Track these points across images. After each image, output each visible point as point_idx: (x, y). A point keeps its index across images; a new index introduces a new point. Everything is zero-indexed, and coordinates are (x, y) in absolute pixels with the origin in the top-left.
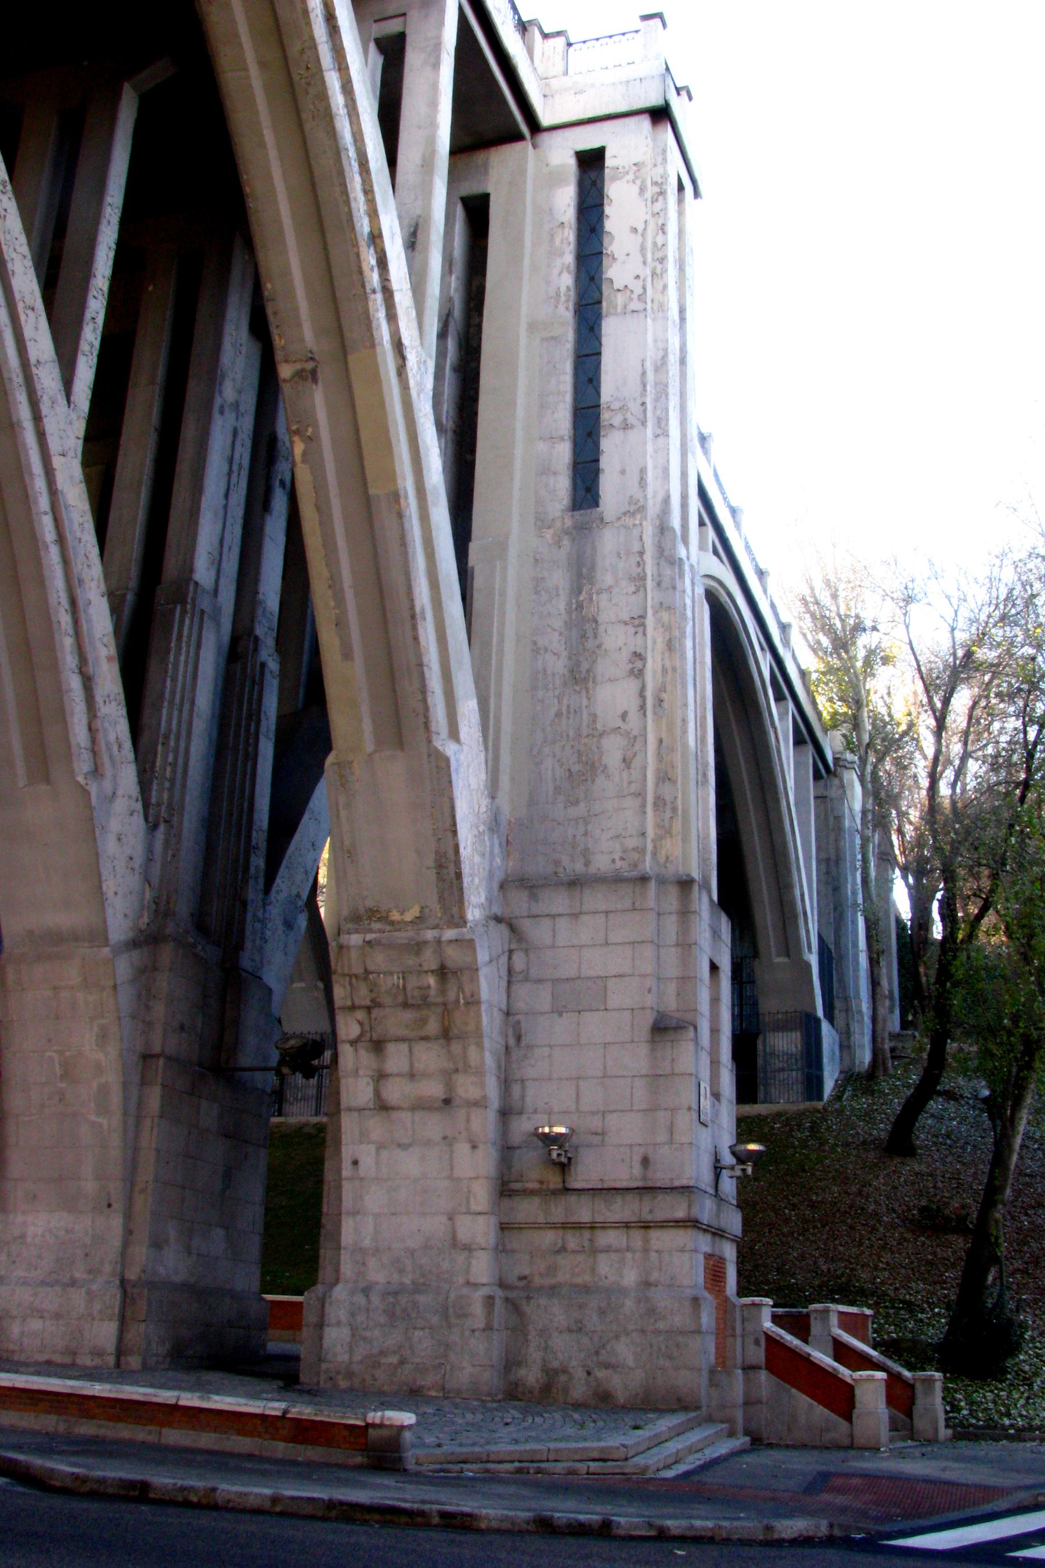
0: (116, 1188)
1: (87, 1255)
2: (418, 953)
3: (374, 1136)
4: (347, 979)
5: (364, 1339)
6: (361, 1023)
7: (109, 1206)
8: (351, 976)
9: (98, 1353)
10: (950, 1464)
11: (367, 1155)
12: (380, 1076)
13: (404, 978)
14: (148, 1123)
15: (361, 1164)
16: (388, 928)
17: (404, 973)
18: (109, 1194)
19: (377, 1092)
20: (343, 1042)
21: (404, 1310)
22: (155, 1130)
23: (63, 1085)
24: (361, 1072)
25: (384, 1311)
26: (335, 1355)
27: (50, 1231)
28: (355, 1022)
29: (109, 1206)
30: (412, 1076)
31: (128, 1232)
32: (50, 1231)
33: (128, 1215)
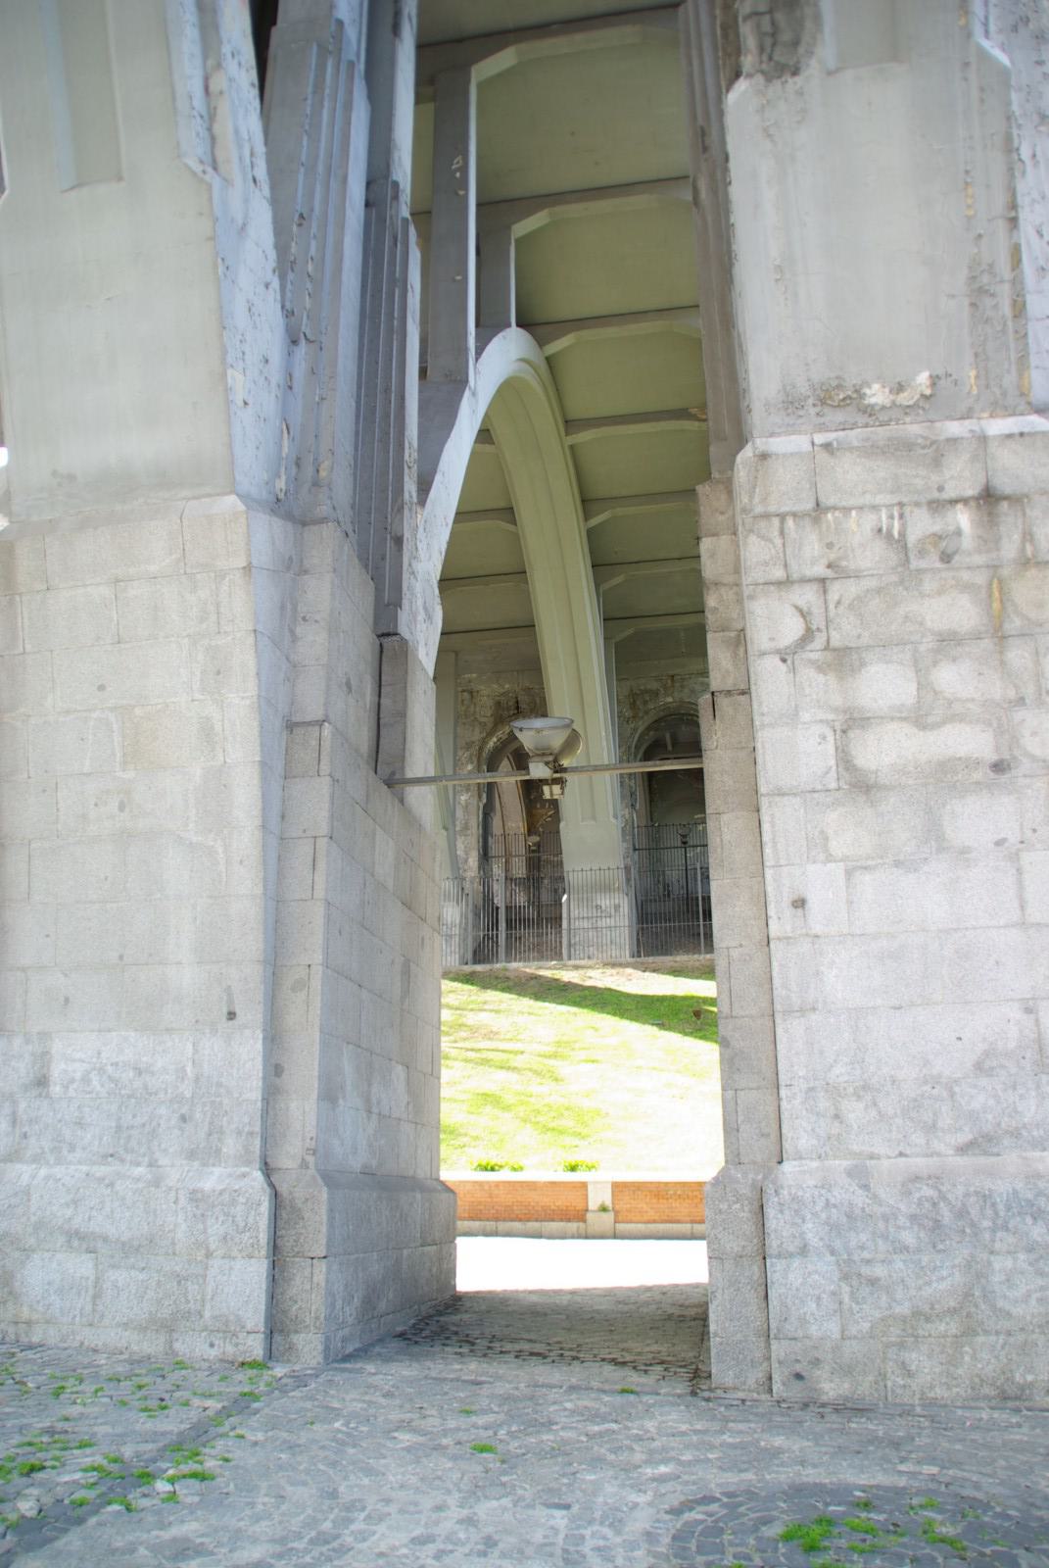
0: (246, 976)
1: (183, 1119)
2: (937, 462)
3: (837, 847)
4: (776, 521)
5: (873, 1282)
6: (804, 614)
7: (232, 1015)
8: (782, 517)
9: (226, 1328)
10: (678, 1370)
11: (821, 883)
12: (852, 722)
13: (901, 516)
14: (304, 850)
15: (813, 903)
16: (861, 419)
17: (901, 505)
18: (228, 990)
19: (845, 760)
20: (763, 654)
21: (962, 1213)
22: (322, 865)
23: (130, 775)
24: (806, 716)
25: (913, 1218)
26: (803, 1321)
27: (101, 1070)
28: (790, 611)
29: (232, 1015)
30: (919, 718)
31: (274, 1071)
32: (101, 1070)
33: (274, 1038)
